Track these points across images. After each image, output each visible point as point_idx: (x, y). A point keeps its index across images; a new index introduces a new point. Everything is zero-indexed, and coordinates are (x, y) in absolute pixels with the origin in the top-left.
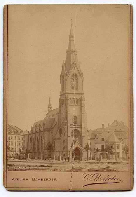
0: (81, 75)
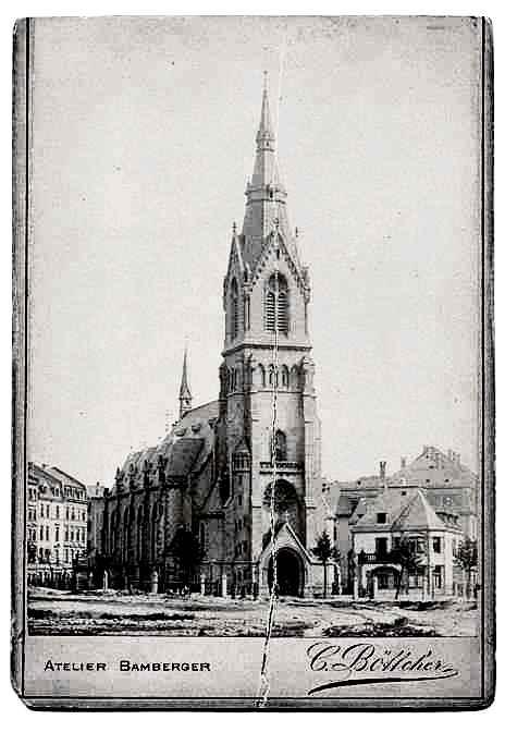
0: (302, 280)
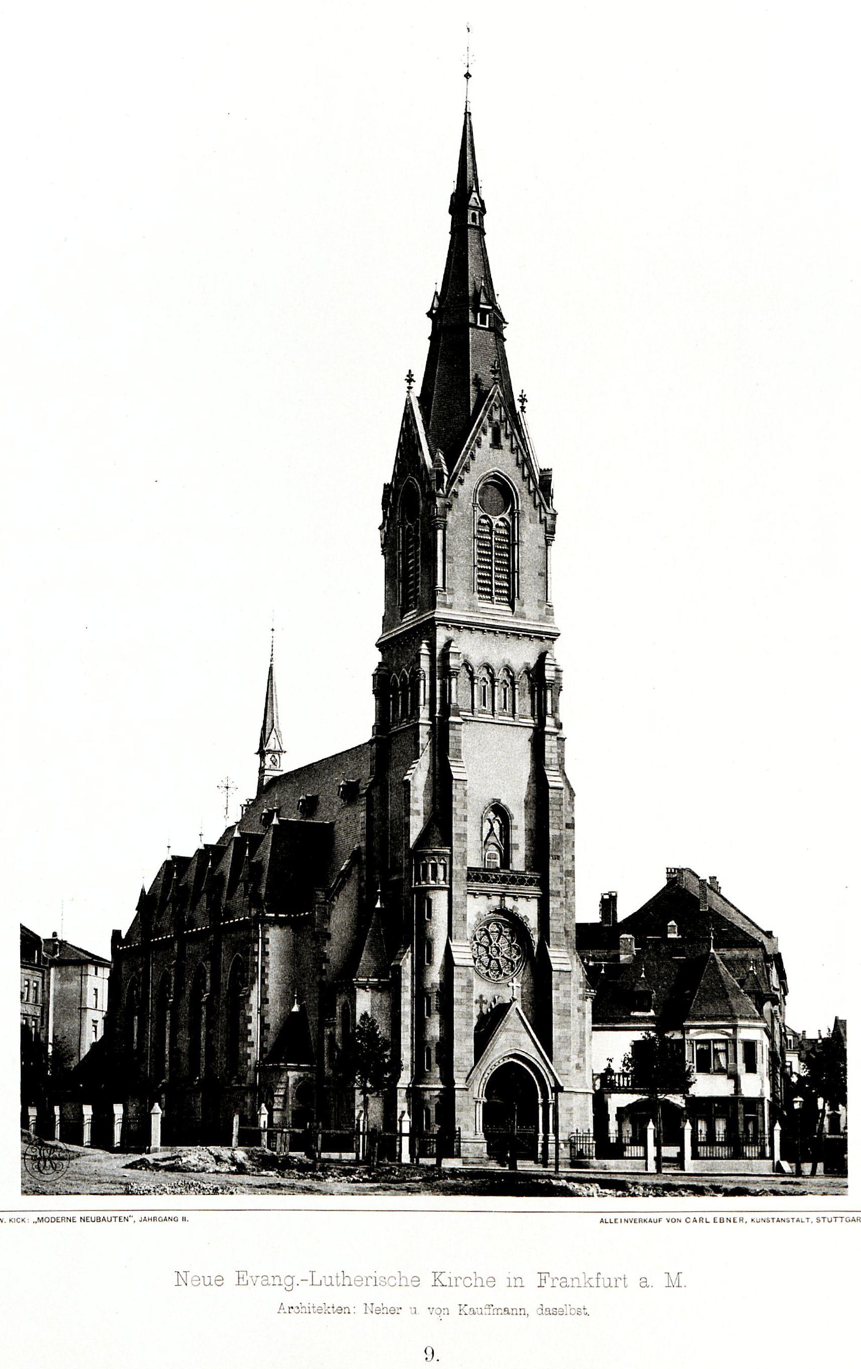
0: (543, 486)
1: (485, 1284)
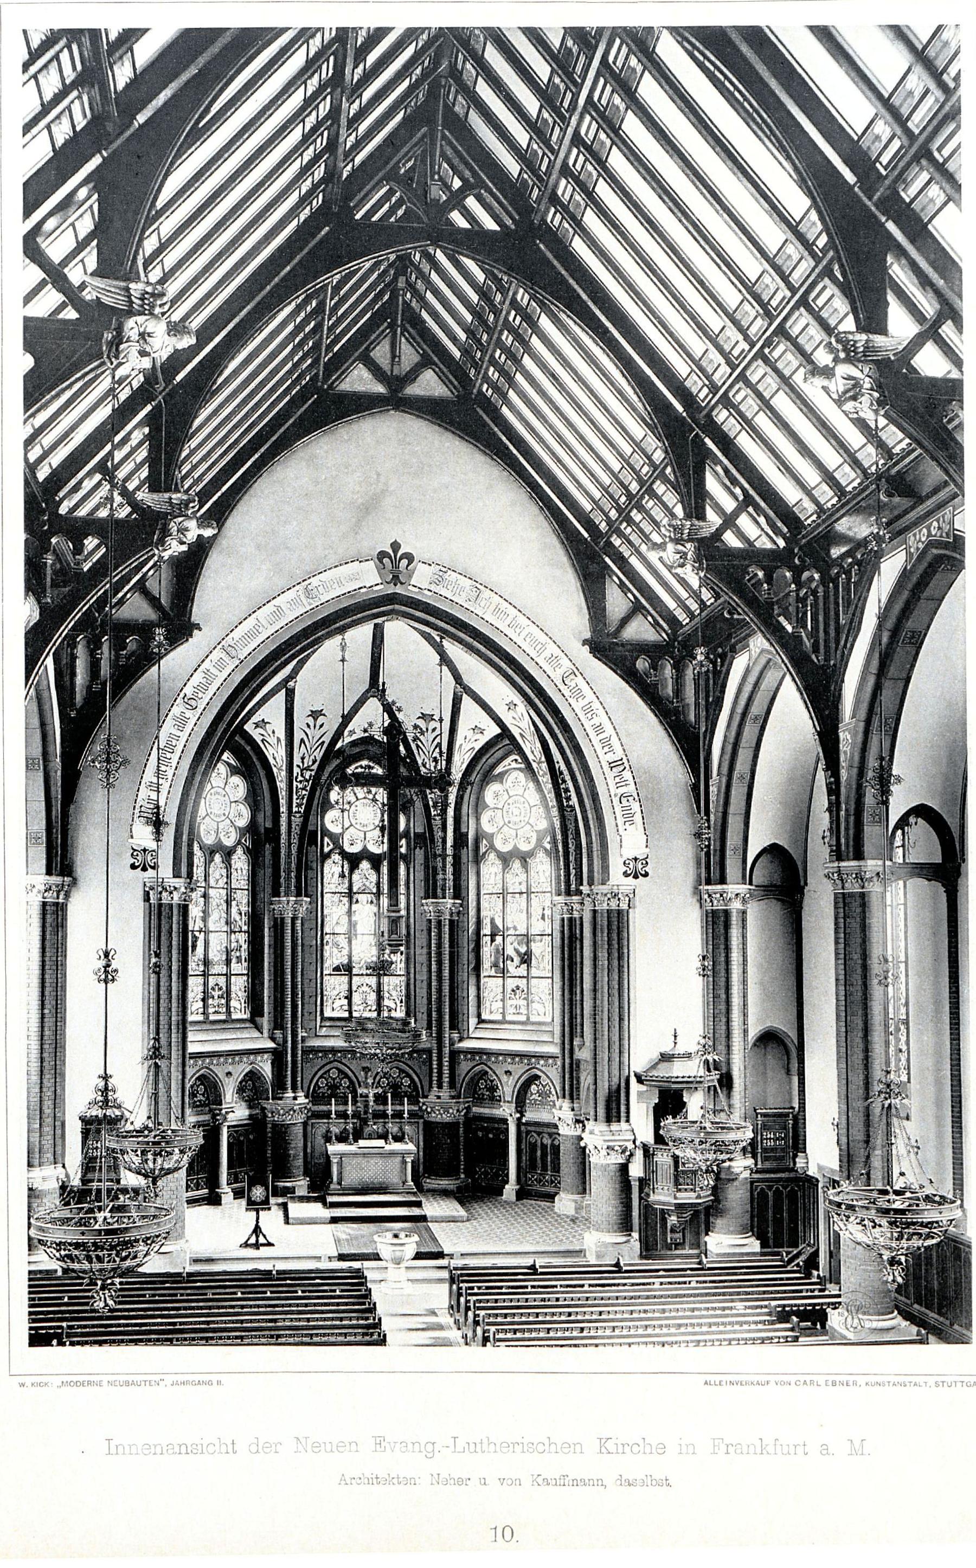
1: (334, 1449)
